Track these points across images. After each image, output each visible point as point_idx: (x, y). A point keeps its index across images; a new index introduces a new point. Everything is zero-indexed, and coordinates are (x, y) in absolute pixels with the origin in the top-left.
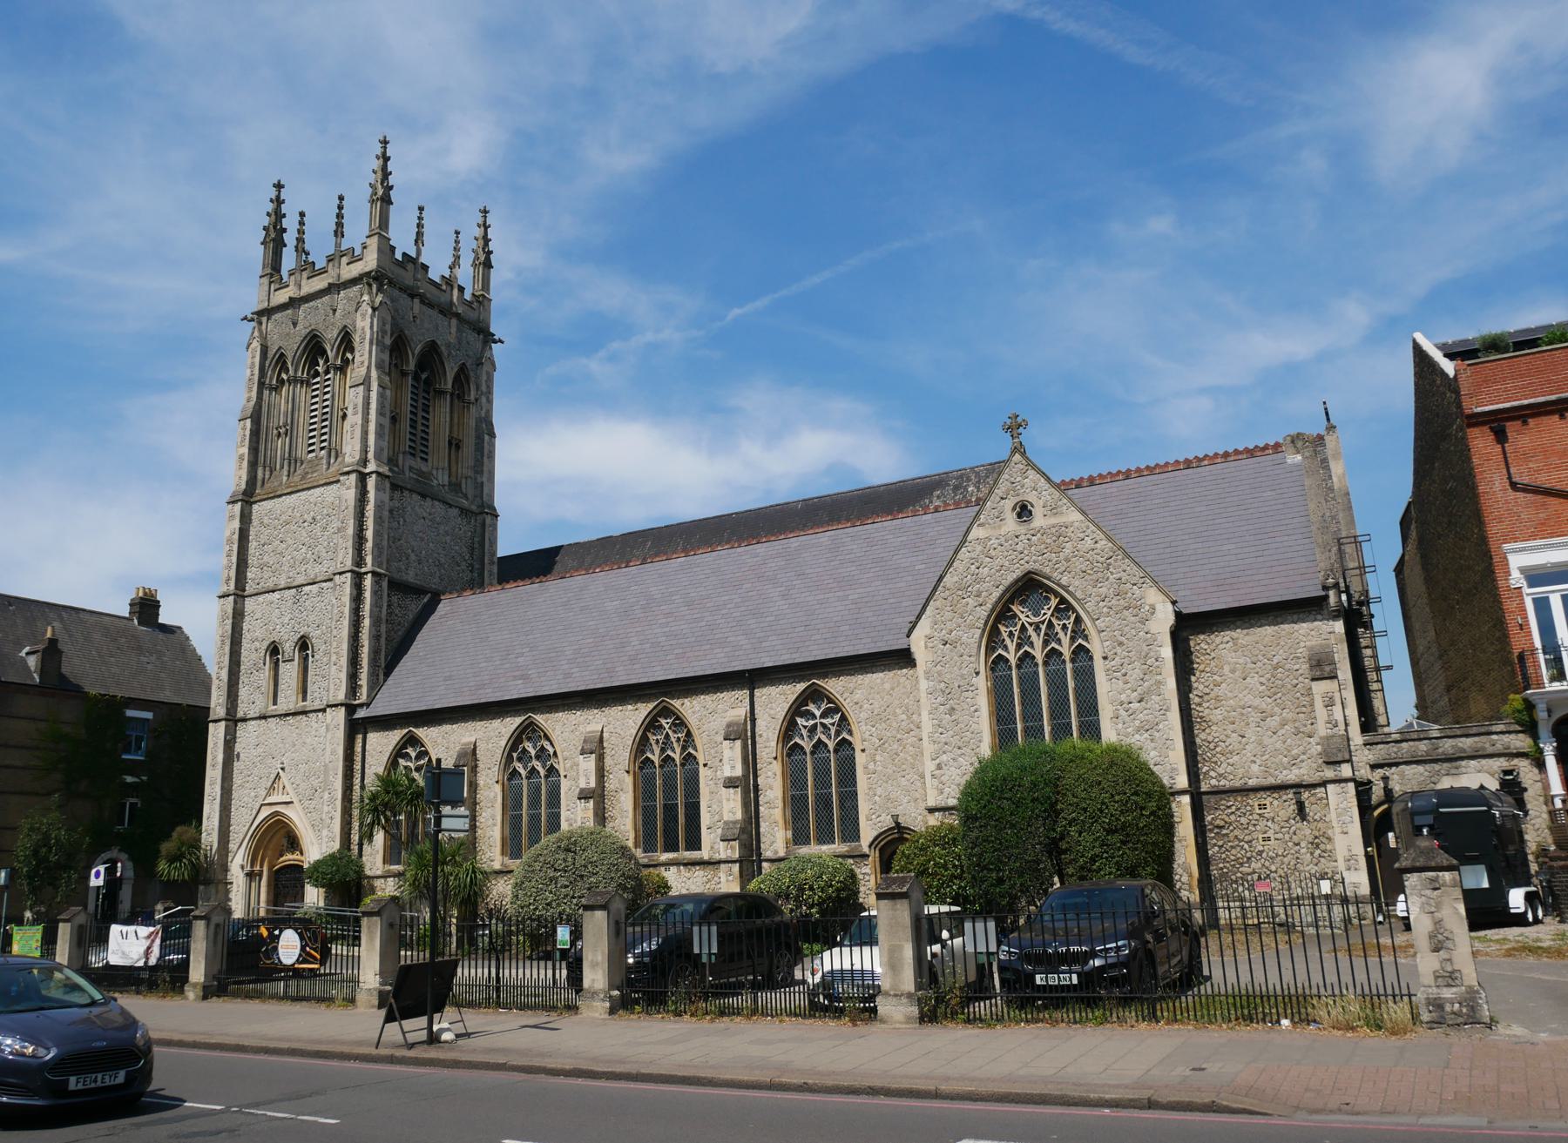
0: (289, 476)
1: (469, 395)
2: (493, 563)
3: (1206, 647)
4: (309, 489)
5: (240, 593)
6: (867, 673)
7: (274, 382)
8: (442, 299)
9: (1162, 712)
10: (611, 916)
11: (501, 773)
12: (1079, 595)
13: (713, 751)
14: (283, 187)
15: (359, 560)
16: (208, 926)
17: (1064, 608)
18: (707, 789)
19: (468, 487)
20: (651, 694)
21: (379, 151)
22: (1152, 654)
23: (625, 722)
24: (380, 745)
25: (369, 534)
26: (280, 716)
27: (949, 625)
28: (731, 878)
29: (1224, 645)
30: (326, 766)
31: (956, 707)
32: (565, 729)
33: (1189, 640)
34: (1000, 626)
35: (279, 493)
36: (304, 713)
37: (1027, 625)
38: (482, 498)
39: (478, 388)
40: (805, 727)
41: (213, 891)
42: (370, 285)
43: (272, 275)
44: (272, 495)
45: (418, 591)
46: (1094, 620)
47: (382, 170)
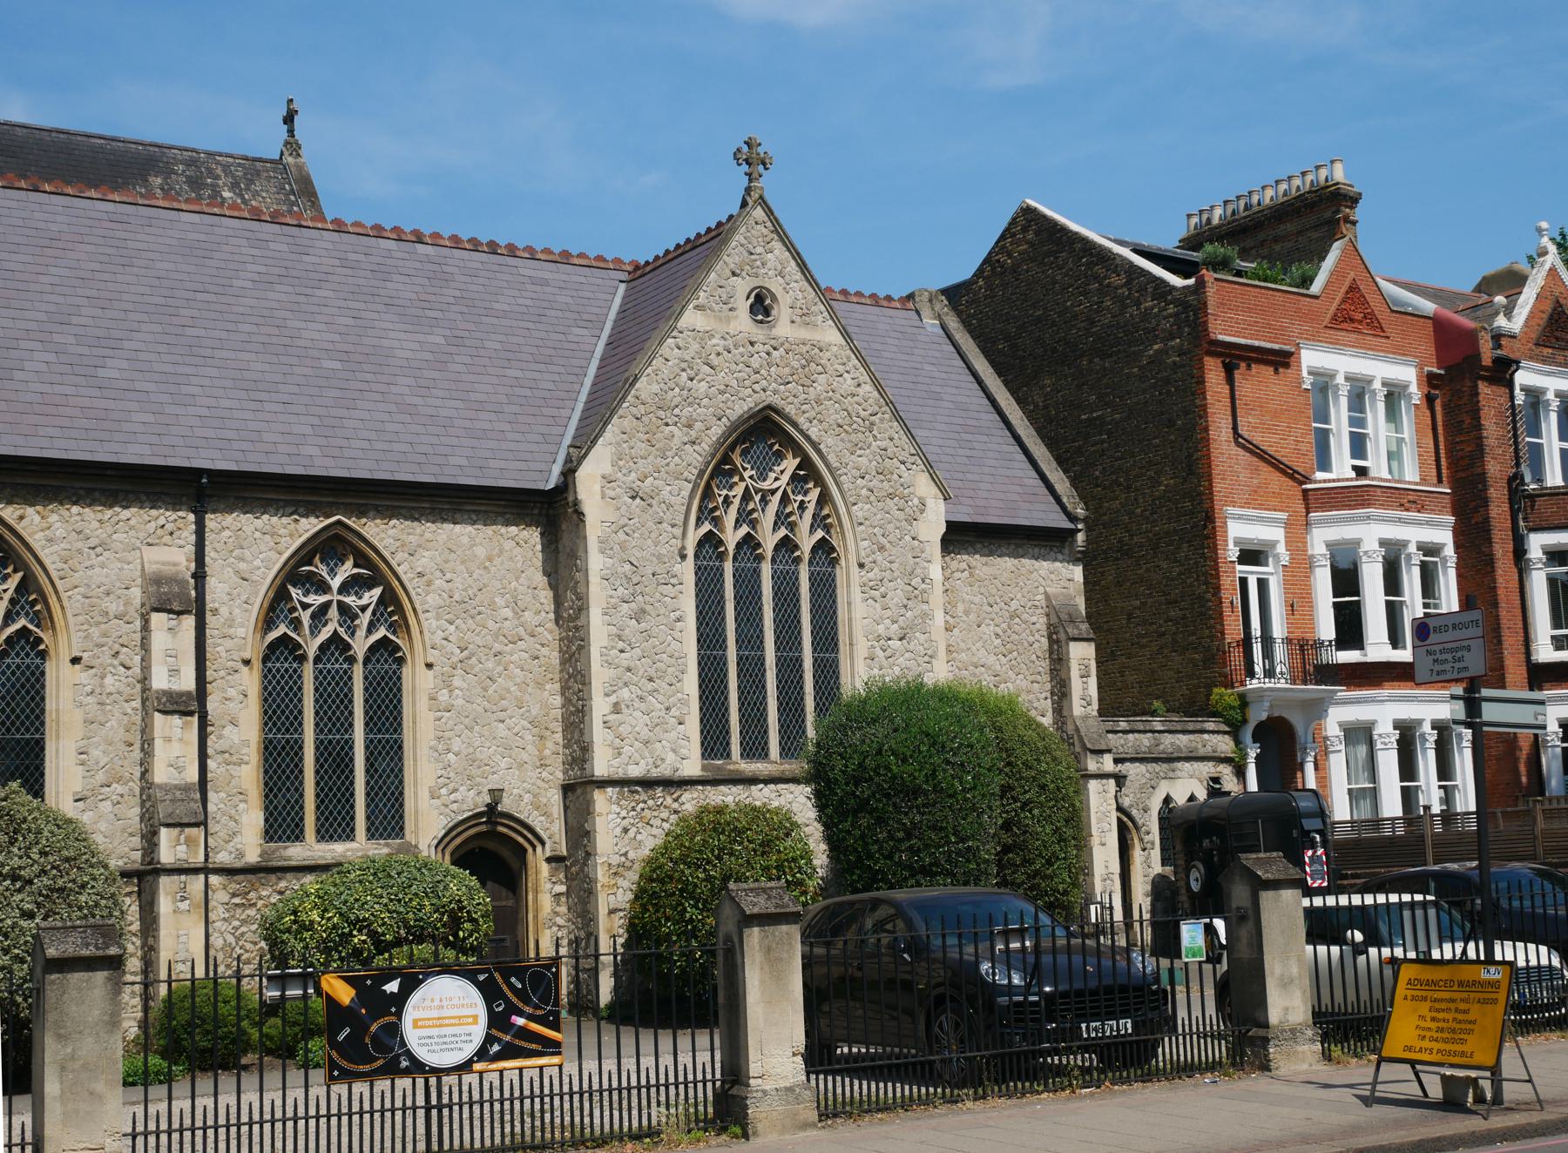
6: (444, 520)
9: (926, 659)
12: (832, 458)
13: (95, 632)
17: (807, 473)
18: (78, 715)
28: (184, 905)
29: (958, 575)
31: (648, 608)
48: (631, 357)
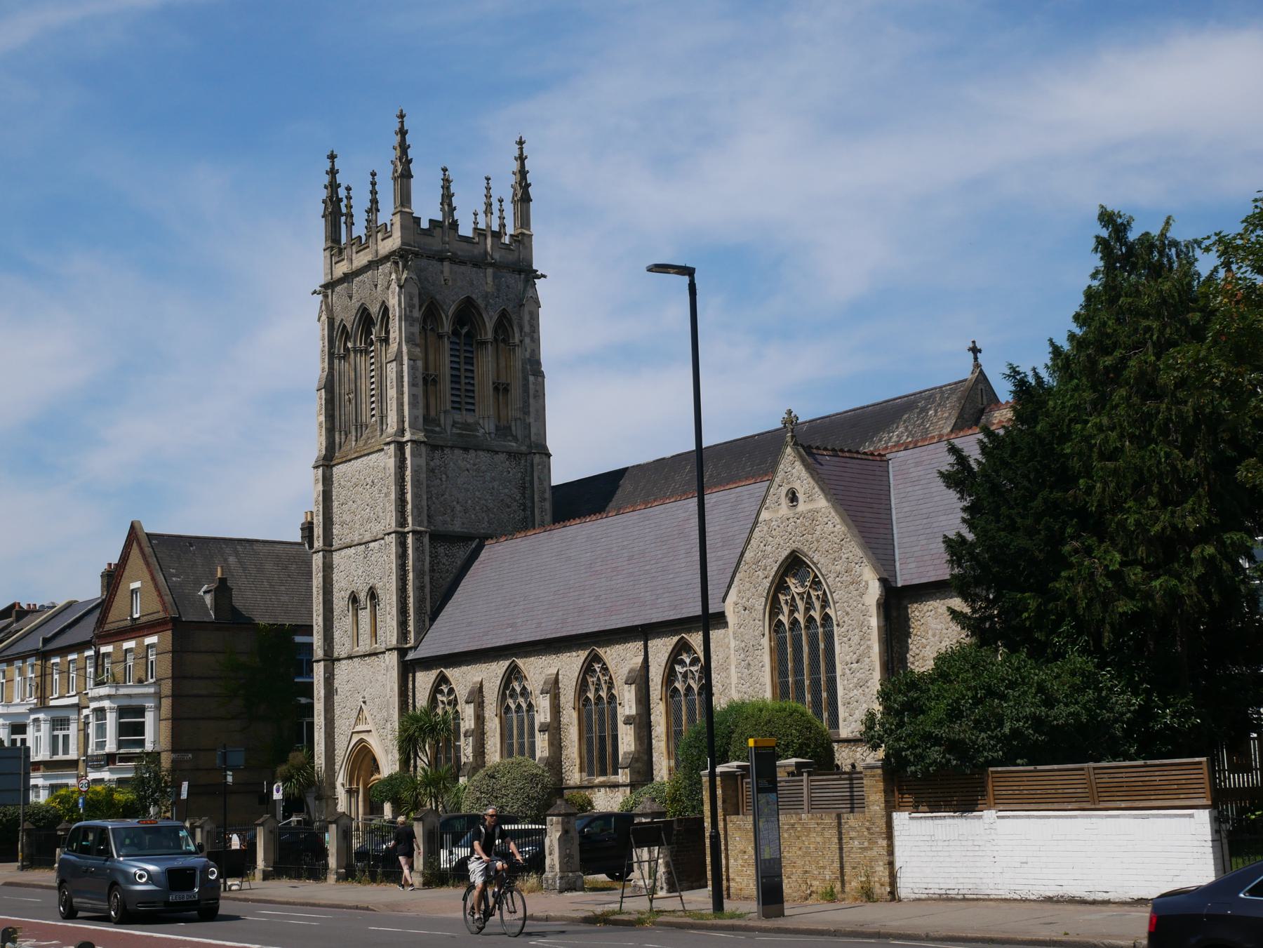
0: (356, 441)
2: (545, 500)
3: (918, 614)
4: (368, 454)
5: (328, 548)
7: (342, 351)
8: (476, 252)
10: (339, 828)
11: (499, 708)
12: (824, 571)
15: (402, 522)
16: (202, 831)
17: (816, 583)
19: (517, 429)
20: (586, 643)
21: (397, 126)
23: (569, 665)
24: (424, 681)
25: (409, 497)
26: (360, 656)
29: (928, 614)
30: (388, 700)
31: (751, 662)
32: (537, 670)
33: (908, 608)
34: (780, 595)
35: (349, 457)
36: (376, 654)
37: (795, 595)
38: (530, 439)
40: (681, 673)
41: (324, 805)
42: (396, 263)
43: (332, 248)
44: (344, 459)
45: (465, 538)
47: (400, 146)
48: (402, 608)
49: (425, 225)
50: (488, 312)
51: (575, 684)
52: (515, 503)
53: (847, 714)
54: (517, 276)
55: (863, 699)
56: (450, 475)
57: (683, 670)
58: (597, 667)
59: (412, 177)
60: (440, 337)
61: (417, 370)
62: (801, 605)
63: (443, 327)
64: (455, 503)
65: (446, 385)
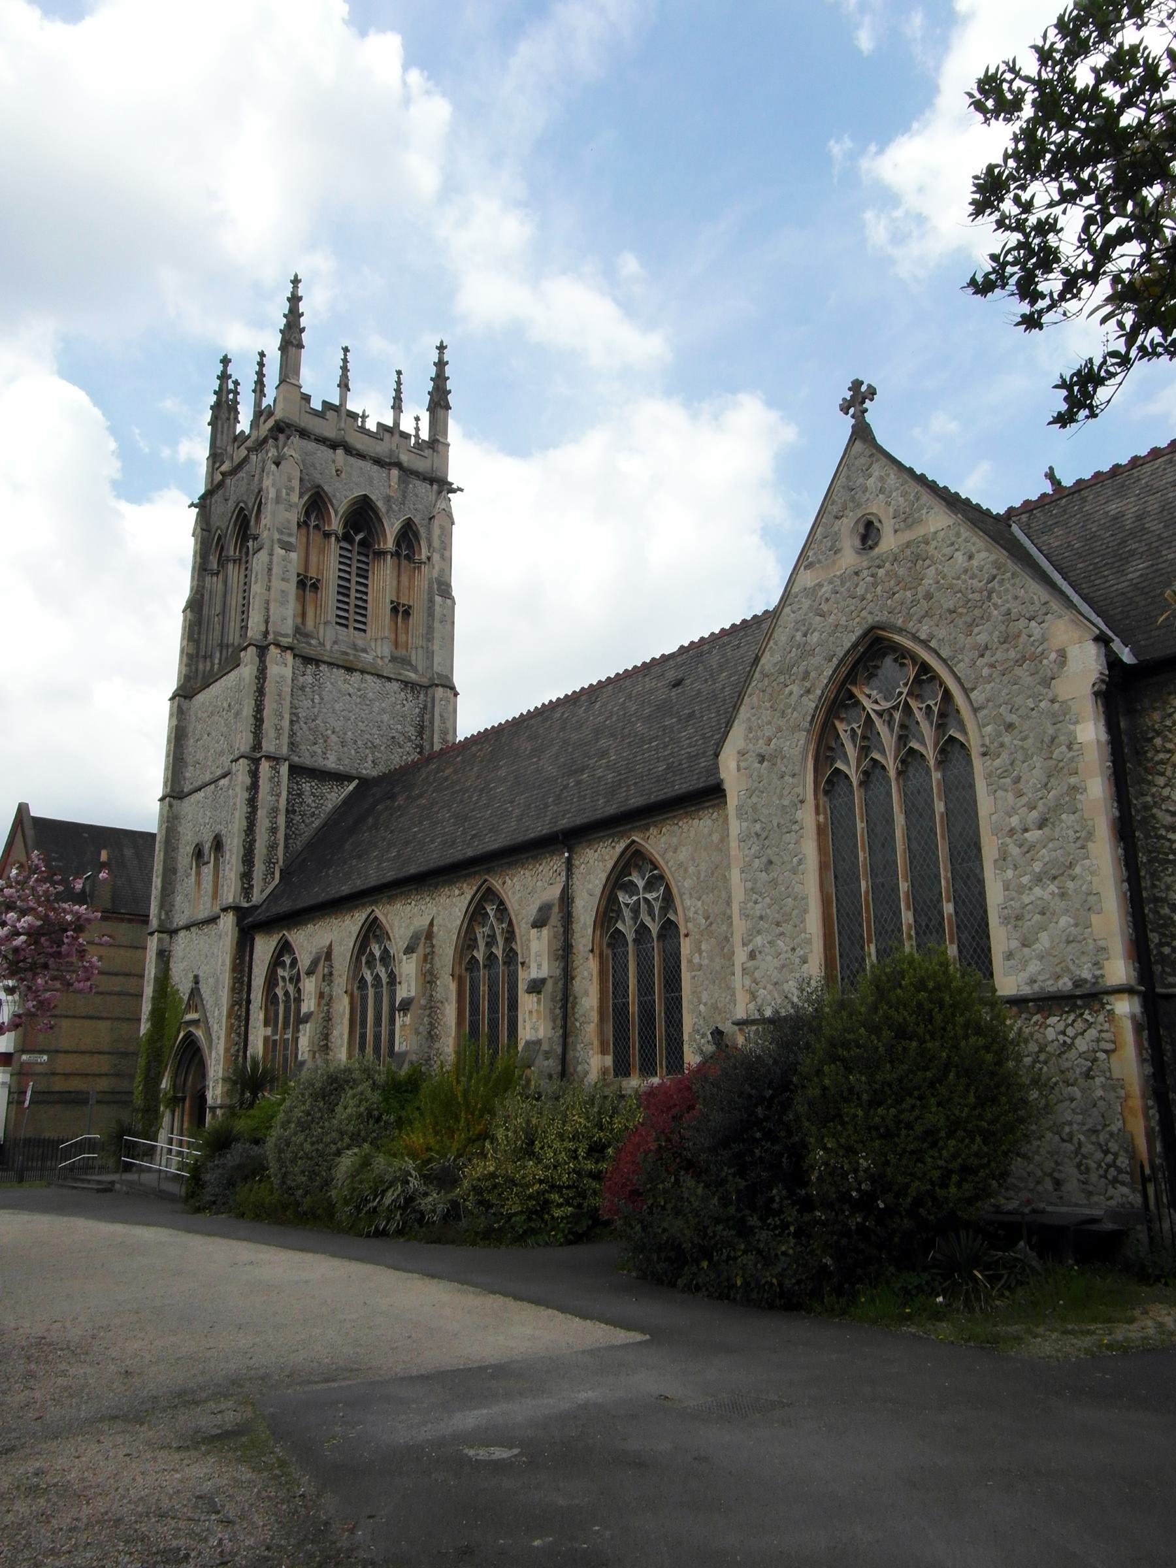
1: (420, 553)
14: (230, 361)
19: (417, 658)
22: (1062, 738)
27: (768, 731)
31: (774, 859)
34: (837, 723)
37: (873, 715)
39: (430, 546)
40: (627, 905)
46: (966, 692)
49: (316, 405)
50: (389, 518)
51: (455, 937)
52: (409, 744)
53: (1014, 944)
54: (429, 486)
55: (1058, 905)
56: (326, 698)
57: (631, 901)
58: (491, 910)
59: (303, 347)
60: (327, 535)
61: (290, 562)
62: (887, 737)
63: (330, 524)
64: (329, 732)
65: (329, 594)
